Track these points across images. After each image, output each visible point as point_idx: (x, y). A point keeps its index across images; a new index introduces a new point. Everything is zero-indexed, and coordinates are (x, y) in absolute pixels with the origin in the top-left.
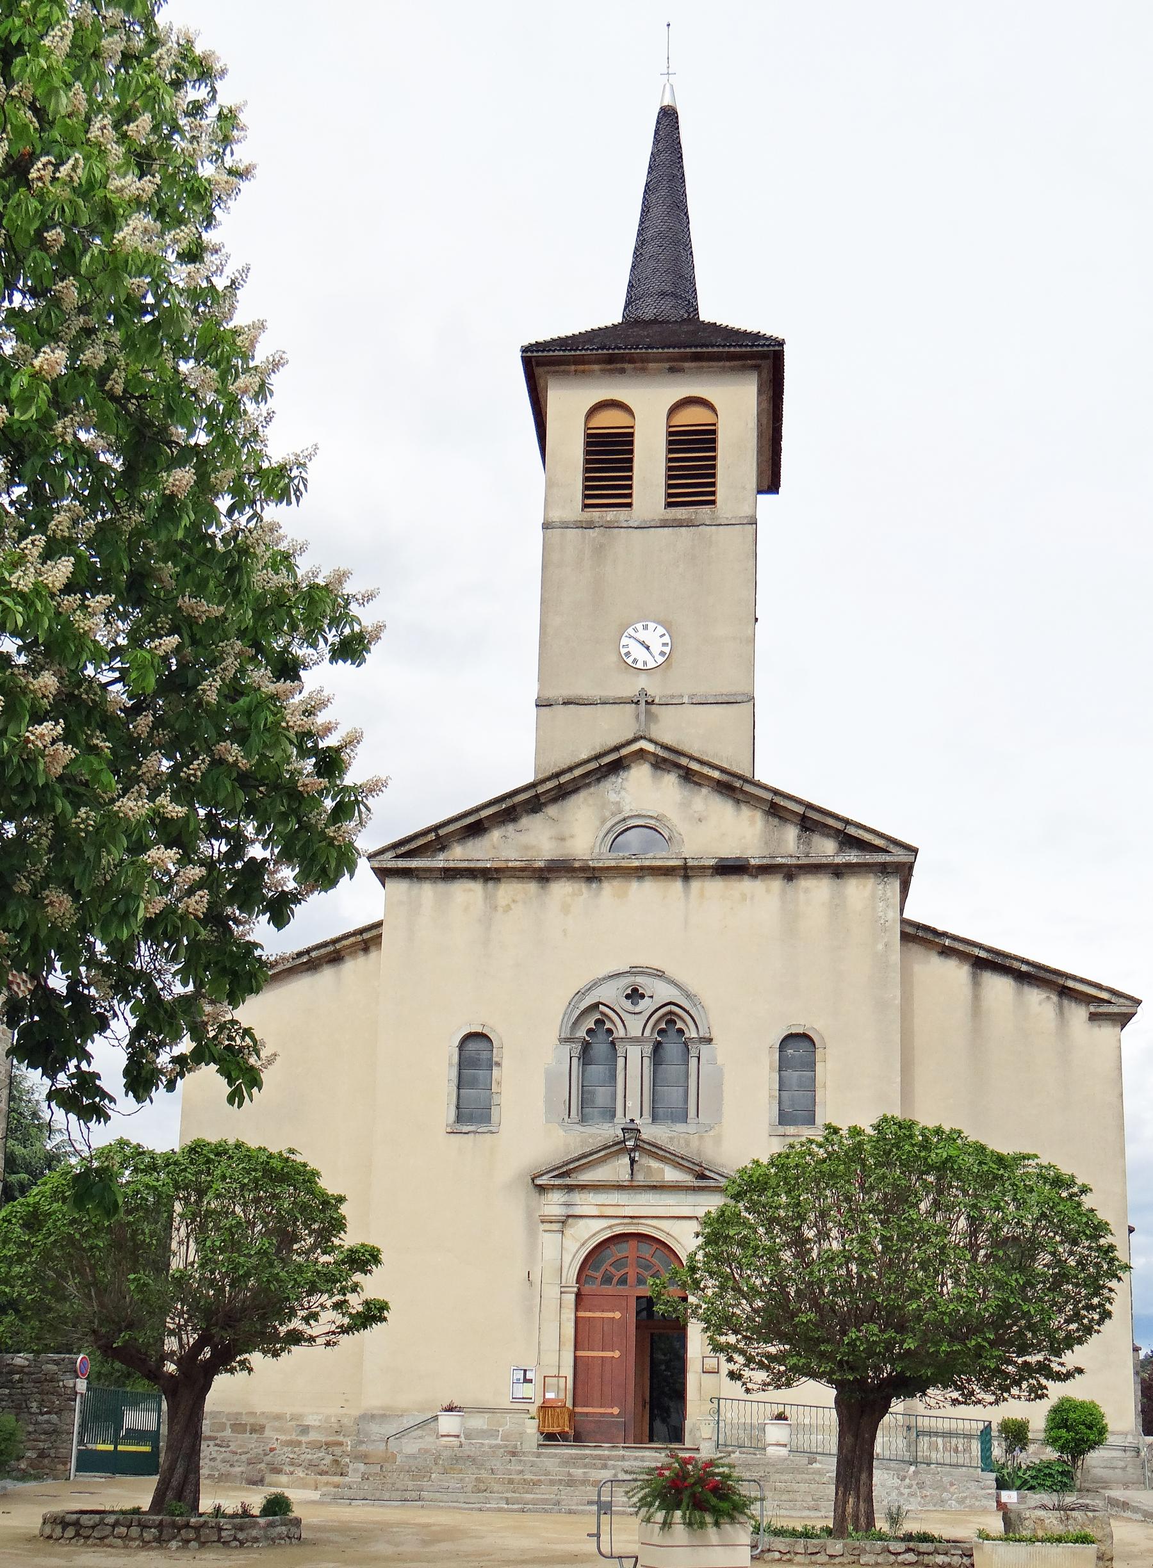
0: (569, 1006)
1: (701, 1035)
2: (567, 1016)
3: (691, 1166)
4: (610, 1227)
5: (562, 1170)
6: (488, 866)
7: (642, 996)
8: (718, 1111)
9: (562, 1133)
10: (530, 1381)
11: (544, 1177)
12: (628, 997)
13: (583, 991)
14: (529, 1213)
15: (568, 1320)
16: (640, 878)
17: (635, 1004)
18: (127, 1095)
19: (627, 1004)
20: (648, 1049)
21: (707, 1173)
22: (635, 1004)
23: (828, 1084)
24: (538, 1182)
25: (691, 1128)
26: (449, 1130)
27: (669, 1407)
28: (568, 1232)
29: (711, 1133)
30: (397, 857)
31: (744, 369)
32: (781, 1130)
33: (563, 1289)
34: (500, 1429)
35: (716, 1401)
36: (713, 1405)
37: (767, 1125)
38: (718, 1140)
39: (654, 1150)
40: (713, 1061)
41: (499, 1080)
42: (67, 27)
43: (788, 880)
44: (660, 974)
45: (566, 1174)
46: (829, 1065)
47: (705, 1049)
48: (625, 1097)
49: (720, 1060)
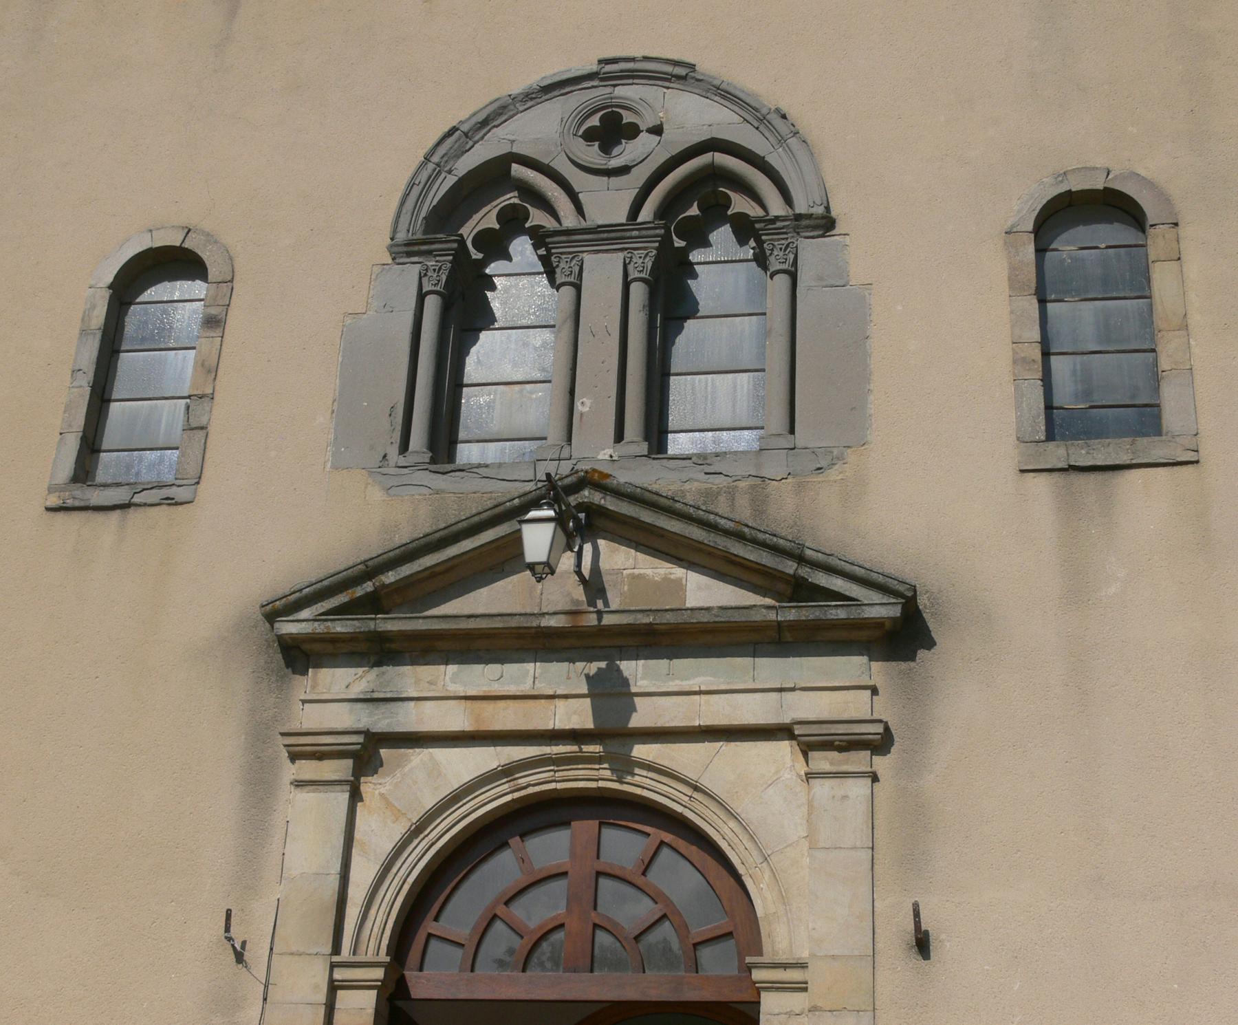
7: (632, 132)
11: (305, 614)
23: (1195, 319)
26: (54, 501)
32: (1057, 454)
34: (561, 973)
40: (838, 281)
46: (1194, 267)
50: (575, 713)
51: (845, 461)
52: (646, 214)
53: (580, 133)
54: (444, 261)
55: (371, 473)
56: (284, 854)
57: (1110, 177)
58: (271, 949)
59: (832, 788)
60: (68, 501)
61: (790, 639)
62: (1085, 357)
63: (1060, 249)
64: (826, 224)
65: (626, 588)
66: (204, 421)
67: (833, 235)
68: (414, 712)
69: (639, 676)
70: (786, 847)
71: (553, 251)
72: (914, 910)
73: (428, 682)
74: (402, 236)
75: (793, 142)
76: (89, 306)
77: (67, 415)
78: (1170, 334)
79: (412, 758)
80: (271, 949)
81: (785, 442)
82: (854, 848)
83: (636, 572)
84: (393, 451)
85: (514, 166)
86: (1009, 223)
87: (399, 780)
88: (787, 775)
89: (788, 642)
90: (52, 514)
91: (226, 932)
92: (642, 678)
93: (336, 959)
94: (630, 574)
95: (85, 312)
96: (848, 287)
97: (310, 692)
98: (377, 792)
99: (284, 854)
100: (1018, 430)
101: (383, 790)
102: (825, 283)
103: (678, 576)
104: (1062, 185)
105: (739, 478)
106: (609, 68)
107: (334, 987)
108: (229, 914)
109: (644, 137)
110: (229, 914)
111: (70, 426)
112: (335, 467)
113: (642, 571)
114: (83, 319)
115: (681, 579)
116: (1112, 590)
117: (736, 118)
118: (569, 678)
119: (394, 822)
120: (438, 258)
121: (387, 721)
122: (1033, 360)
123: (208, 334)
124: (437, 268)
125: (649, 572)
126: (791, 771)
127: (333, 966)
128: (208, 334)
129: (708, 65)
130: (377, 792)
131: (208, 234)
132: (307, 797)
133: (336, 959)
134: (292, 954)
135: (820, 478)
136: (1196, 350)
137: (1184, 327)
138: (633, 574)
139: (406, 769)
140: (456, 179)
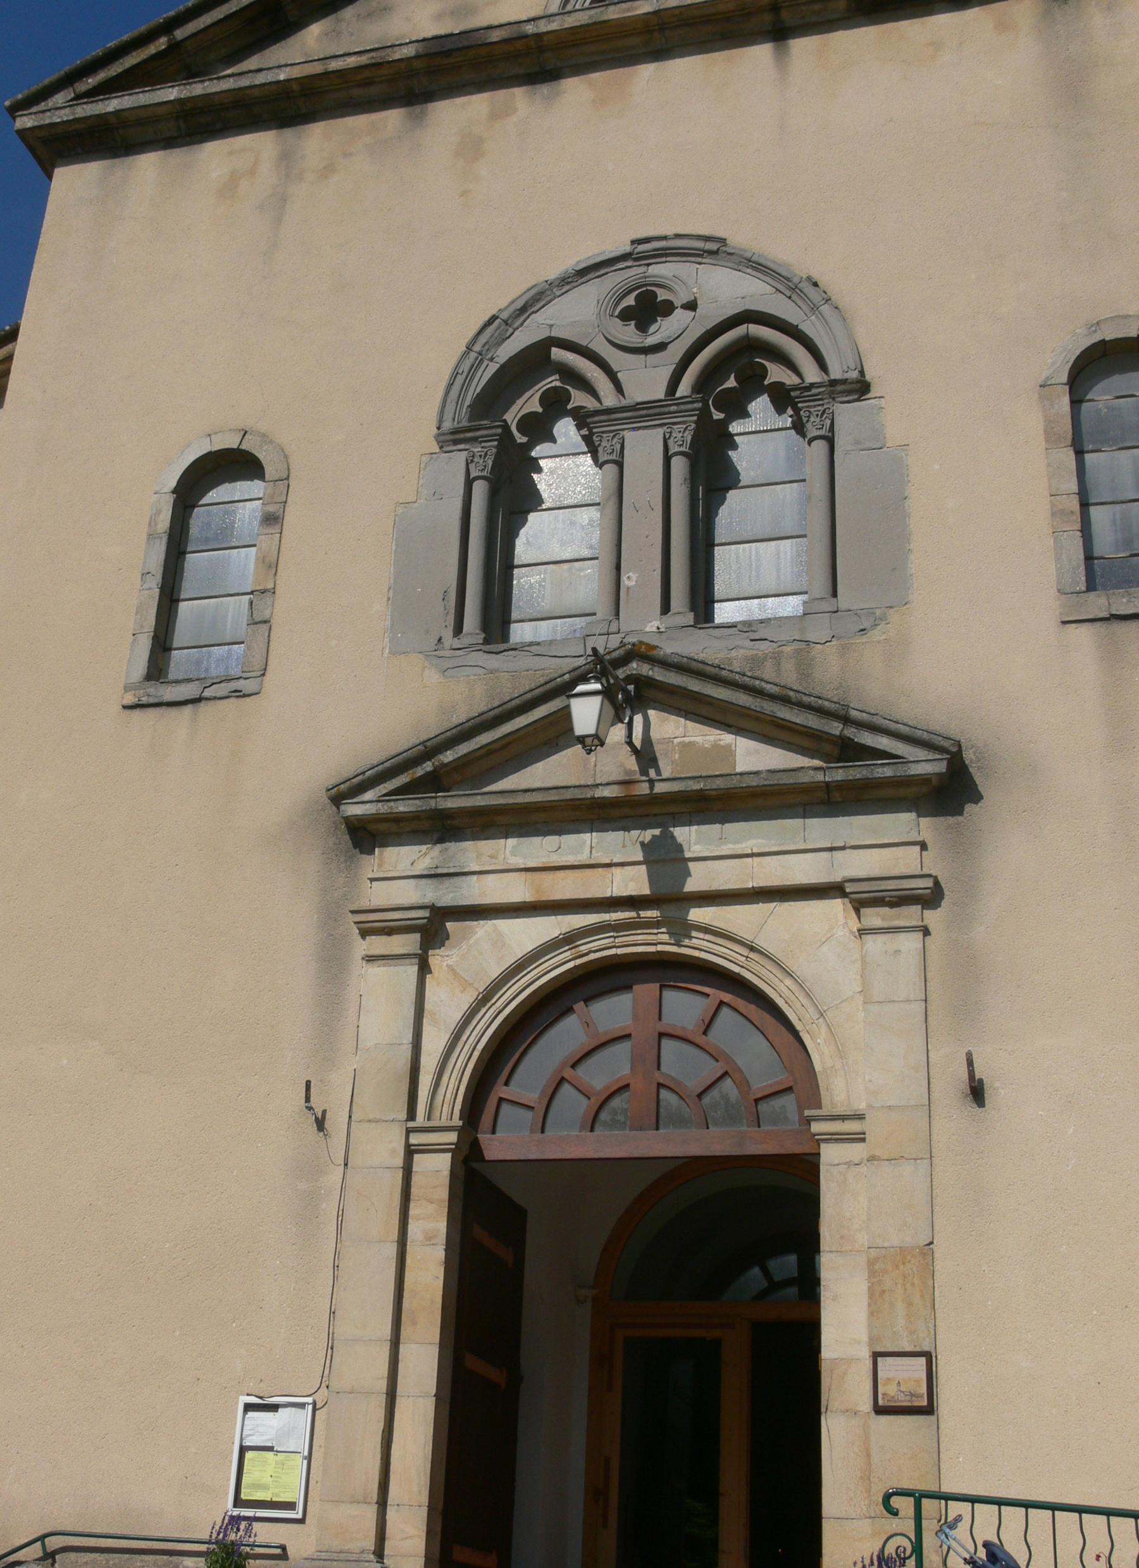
0: (465, 355)
1: (836, 373)
2: (460, 380)
3: (812, 721)
4: (569, 939)
6: (282, 77)
7: (667, 309)
9: (433, 677)
12: (626, 315)
13: (504, 316)
14: (329, 915)
15: (429, 1238)
16: (660, 54)
17: (643, 327)
18: (324, 1112)
19: (628, 333)
20: (683, 435)
22: (643, 327)
24: (354, 810)
26: (130, 699)
27: (515, 110)
28: (438, 959)
29: (876, 635)
30: (77, 97)
31: (725, 1078)
32: (1098, 604)
33: (415, 1139)
35: (905, 1505)
36: (894, 1524)
37: (1053, 592)
39: (694, 685)
45: (435, 782)
47: (847, 415)
49: (894, 434)
50: (631, 880)
58: (350, 1117)
60: (143, 699)
62: (1124, 506)
63: (1096, 398)
64: (861, 388)
66: (266, 614)
68: (476, 885)
71: (594, 430)
74: (447, 425)
75: (825, 309)
79: (478, 929)
82: (908, 1001)
83: (687, 739)
84: (448, 634)
87: (465, 951)
90: (128, 712)
92: (695, 844)
93: (411, 1124)
94: (680, 742)
96: (885, 449)
101: (450, 962)
106: (641, 248)
107: (410, 1152)
109: (679, 313)
111: (142, 626)
113: (692, 739)
114: (150, 525)
118: (624, 846)
119: (462, 992)
120: (483, 444)
121: (451, 895)
124: (483, 454)
127: (409, 1131)
129: (739, 238)
130: (444, 964)
132: (377, 971)
133: (411, 1124)
135: (864, 639)
138: (684, 742)
139: (472, 941)
140: (498, 366)
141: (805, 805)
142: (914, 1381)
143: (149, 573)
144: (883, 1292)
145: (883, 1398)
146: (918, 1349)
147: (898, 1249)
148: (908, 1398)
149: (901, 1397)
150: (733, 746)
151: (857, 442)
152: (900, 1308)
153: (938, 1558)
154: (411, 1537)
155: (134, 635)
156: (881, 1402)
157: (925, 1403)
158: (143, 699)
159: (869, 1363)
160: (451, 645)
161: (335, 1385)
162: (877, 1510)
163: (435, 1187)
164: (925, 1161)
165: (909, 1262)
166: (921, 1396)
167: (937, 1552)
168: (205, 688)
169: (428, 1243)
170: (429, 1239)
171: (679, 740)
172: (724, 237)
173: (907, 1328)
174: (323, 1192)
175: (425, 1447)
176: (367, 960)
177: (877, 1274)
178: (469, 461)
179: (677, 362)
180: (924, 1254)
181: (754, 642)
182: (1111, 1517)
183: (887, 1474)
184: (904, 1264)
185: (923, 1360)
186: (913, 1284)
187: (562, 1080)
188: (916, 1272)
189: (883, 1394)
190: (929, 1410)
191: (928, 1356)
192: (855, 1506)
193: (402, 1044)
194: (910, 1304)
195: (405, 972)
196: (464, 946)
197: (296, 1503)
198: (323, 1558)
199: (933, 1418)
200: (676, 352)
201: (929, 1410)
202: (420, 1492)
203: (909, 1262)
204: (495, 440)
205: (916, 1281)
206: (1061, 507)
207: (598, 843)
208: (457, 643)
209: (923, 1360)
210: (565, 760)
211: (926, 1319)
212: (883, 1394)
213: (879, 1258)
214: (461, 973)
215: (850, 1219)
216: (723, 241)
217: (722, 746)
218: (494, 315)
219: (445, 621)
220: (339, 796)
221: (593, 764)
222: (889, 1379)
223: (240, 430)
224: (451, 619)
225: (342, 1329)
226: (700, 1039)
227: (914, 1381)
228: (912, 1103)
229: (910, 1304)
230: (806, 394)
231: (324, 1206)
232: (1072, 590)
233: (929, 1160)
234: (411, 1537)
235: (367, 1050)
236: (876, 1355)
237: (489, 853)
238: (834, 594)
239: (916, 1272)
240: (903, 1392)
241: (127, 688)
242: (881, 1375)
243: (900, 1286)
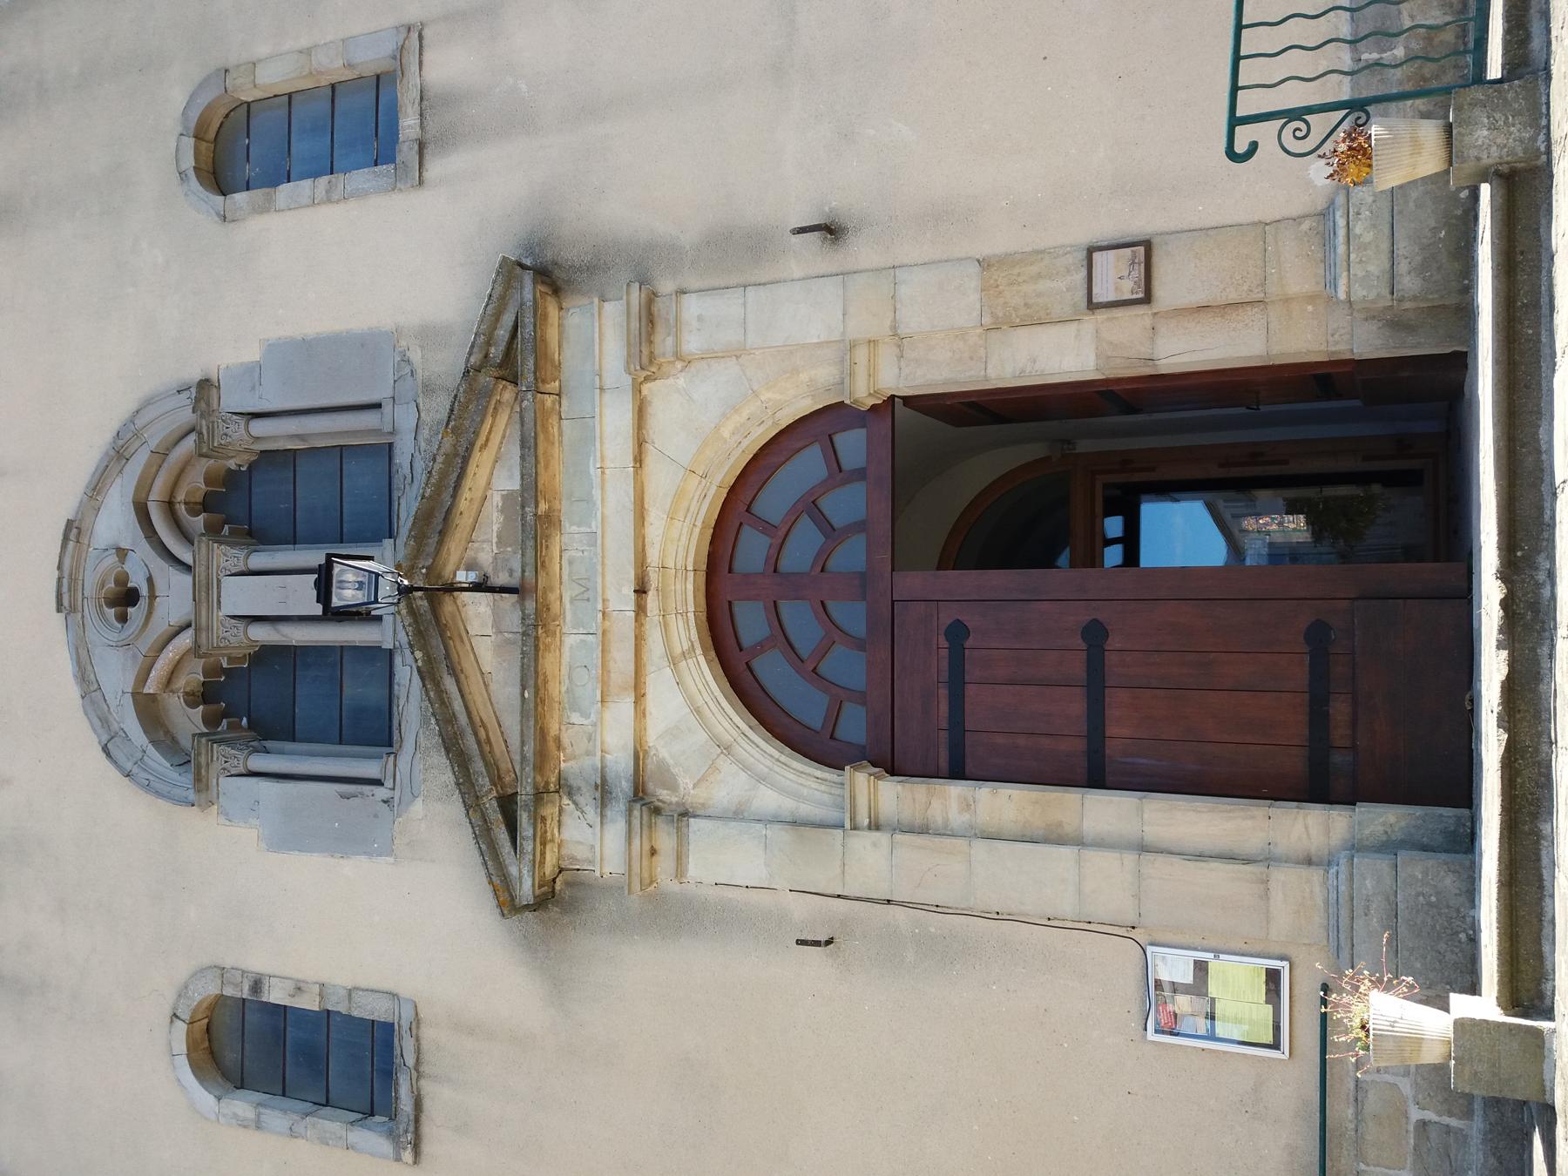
5: (495, 816)
7: (122, 580)
8: (366, 345)
9: (418, 807)
10: (1201, 968)
11: (513, 870)
21: (496, 352)
23: (304, 42)
25: (405, 419)
26: (408, 1156)
29: (416, 356)
32: (407, 152)
34: (1416, 1114)
38: (429, 335)
40: (254, 372)
41: (290, 985)
42: (1503, 1074)
43: (1149, 303)
44: (74, 531)
46: (262, 50)
47: (232, 399)
48: (970, 601)
50: (620, 591)
51: (406, 349)
52: (187, 557)
53: (120, 626)
54: (217, 752)
55: (399, 816)
56: (747, 887)
57: (185, 133)
58: (839, 896)
59: (691, 331)
60: (409, 1138)
61: (557, 383)
62: (336, 146)
63: (247, 178)
64: (205, 387)
65: (509, 549)
66: (344, 993)
67: (219, 380)
68: (615, 755)
69: (589, 530)
70: (745, 376)
71: (215, 645)
72: (798, 233)
73: (589, 742)
74: (191, 795)
75: (139, 423)
76: (234, 1121)
77: (330, 1142)
78: (313, 63)
79: (660, 757)
80: (839, 896)
81: (387, 408)
82: (745, 304)
83: (495, 540)
84: (381, 793)
85: (146, 691)
86: (217, 219)
87: (681, 769)
88: (681, 381)
89: (560, 386)
90: (423, 1157)
91: (820, 946)
92: (590, 527)
93: (848, 825)
94: (497, 547)
95: (240, 1125)
96: (262, 362)
97: (594, 866)
98: (692, 792)
99: (747, 887)
100: (386, 191)
101: (691, 786)
102: (257, 384)
103: (499, 499)
104: (189, 175)
105: (417, 448)
106: (66, 602)
107: (875, 826)
108: (801, 942)
109: (127, 567)
110: (801, 942)
111: (340, 1138)
112: (390, 853)
113: (495, 535)
114: (245, 1127)
115: (503, 496)
116: (524, 87)
117: (118, 481)
118: (588, 600)
119: (720, 772)
120: (215, 759)
121: (623, 783)
122: (329, 182)
123: (266, 992)
124: (224, 759)
125: (495, 528)
126: (678, 378)
127: (854, 828)
128: (266, 992)
129: (66, 508)
130: (692, 792)
131: (180, 996)
132: (694, 870)
133: (848, 825)
134: (843, 873)
135: (420, 371)
136: (329, 38)
137: (307, 52)
138: (496, 543)
139: (671, 762)
140: (150, 746)
141: (561, 418)
142: (1118, 261)
143: (291, 1128)
144: (1026, 304)
145: (1137, 293)
146: (1085, 263)
147: (983, 293)
148: (1136, 267)
149: (1135, 274)
150: (503, 493)
151: (253, 388)
152: (1043, 285)
153: (1307, 222)
154: (1306, 828)
155: (348, 1148)
156: (1141, 295)
157: (1141, 249)
158: (409, 1138)
159: (1101, 316)
160: (390, 789)
161: (1131, 918)
162: (1257, 290)
163: (914, 800)
164: (897, 273)
165: (996, 280)
166: (1134, 254)
167: (1300, 224)
168: (405, 1065)
169: (972, 807)
170: (968, 806)
171: (495, 548)
172: (66, 521)
173: (1064, 276)
174: (917, 931)
175: (1199, 812)
176: (681, 876)
177: (1007, 314)
178: (229, 774)
179: (167, 566)
180: (988, 266)
181: (415, 479)
182: (1240, 85)
183: (1218, 283)
184: (997, 286)
185: (1096, 256)
186: (1019, 275)
187: (814, 670)
188: (1007, 273)
189: (1133, 294)
190: (1148, 245)
191: (1091, 251)
192: (1253, 321)
193: (766, 835)
194: (1039, 276)
195: (695, 832)
196: (675, 770)
197: (1267, 969)
198: (1335, 933)
199: (1155, 241)
200: (159, 566)
201: (1148, 245)
202: (1253, 817)
203: (996, 280)
204: (212, 746)
205: (1016, 271)
206: (324, 192)
207: (583, 627)
208: (388, 783)
209: (1096, 256)
210: (504, 664)
211: (1055, 258)
212: (1133, 294)
213: (992, 313)
214: (702, 773)
215: (954, 351)
216: (69, 524)
217: (503, 504)
218: (103, 748)
219: (368, 796)
220: (503, 915)
221: (510, 635)
222: (1116, 289)
223: (172, 1022)
224: (367, 789)
225: (1066, 906)
226: (781, 533)
227: (1118, 261)
228: (841, 292)
229: (1039, 276)
230: (206, 437)
231: (933, 930)
232: (393, 176)
233: (897, 271)
234: (1306, 828)
235: (770, 875)
236: (1092, 306)
237: (587, 741)
238: (378, 406)
239: (1007, 273)
240: (1130, 272)
241: (398, 1159)
242: (1112, 297)
243: (1020, 288)
